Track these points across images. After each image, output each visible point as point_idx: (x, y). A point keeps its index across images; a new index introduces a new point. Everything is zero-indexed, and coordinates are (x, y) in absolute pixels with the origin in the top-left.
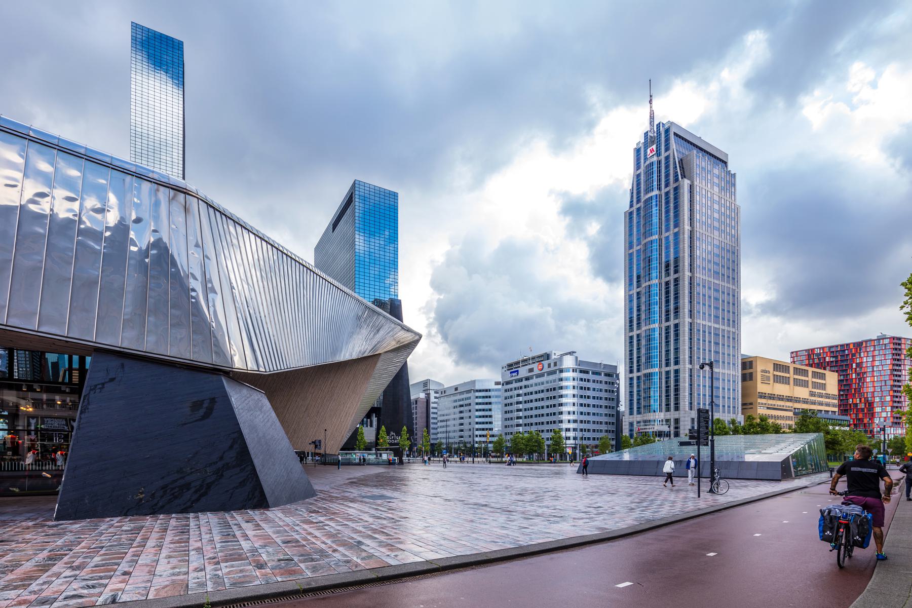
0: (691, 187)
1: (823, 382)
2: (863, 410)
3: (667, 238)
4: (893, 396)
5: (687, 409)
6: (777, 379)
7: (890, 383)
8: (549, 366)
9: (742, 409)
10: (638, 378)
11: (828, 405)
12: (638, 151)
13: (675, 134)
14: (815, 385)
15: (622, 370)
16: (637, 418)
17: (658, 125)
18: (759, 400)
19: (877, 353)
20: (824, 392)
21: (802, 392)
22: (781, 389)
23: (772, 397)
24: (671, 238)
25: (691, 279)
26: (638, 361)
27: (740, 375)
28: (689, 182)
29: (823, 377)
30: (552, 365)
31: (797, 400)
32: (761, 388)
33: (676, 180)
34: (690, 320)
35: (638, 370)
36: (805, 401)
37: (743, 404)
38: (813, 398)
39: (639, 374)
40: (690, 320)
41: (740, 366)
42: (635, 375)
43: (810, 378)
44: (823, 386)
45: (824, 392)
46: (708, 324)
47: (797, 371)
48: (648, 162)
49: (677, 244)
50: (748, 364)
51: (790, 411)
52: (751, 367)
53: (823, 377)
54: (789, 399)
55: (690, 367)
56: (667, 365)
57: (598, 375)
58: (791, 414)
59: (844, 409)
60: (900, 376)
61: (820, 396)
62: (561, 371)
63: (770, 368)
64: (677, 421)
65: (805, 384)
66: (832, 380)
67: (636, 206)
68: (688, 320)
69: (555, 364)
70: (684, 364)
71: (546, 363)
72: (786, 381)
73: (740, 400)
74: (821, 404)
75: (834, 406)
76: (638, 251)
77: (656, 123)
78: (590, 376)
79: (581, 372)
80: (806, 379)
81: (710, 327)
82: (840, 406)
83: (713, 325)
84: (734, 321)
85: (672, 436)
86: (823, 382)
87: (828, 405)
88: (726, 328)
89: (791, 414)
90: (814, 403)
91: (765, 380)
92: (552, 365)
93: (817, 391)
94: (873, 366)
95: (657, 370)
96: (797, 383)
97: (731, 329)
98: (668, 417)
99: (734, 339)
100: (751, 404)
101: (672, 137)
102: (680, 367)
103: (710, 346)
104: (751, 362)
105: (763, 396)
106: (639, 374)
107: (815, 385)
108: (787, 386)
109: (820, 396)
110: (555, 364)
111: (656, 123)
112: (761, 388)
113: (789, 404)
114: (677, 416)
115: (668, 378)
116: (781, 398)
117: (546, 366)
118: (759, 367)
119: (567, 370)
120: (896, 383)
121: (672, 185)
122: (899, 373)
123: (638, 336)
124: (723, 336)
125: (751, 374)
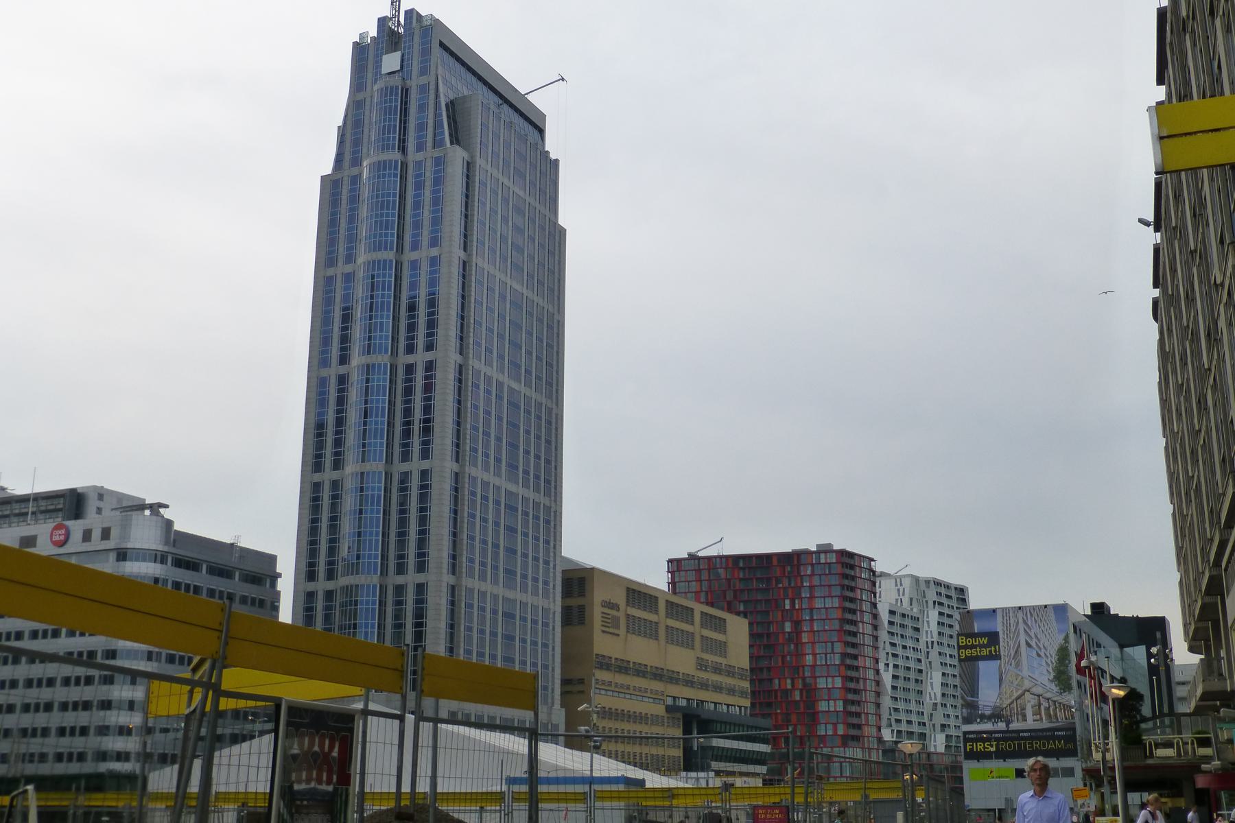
0: (469, 165)
3: (414, 265)
4: (846, 702)
6: (636, 627)
7: (839, 647)
8: (87, 535)
9: (562, 694)
10: (329, 595)
12: (360, 50)
13: (442, 44)
15: (287, 569)
17: (410, 13)
19: (816, 581)
21: (682, 660)
22: (641, 650)
23: (623, 667)
24: (424, 268)
25: (461, 369)
26: (334, 507)
27: (559, 610)
28: (466, 155)
29: (720, 625)
30: (96, 534)
31: (672, 678)
32: (604, 645)
33: (438, 143)
35: (330, 575)
36: (689, 682)
37: (565, 682)
40: (456, 467)
41: (559, 589)
42: (321, 585)
43: (696, 628)
44: (721, 648)
46: (488, 587)
47: (674, 609)
49: (438, 181)
50: (578, 582)
52: (582, 594)
53: (720, 625)
56: (410, 349)
59: (764, 696)
61: (717, 669)
63: (620, 598)
65: (685, 640)
66: (738, 630)
67: (348, 171)
68: (450, 465)
69: (106, 534)
71: (77, 527)
72: (650, 630)
73: (558, 671)
74: (718, 688)
75: (743, 694)
76: (415, 246)
77: (404, 7)
83: (500, 591)
84: (548, 482)
88: (531, 495)
89: (660, 710)
90: (704, 686)
91: (611, 624)
92: (96, 534)
94: (811, 609)
96: (675, 637)
99: (547, 522)
100: (581, 681)
103: (496, 556)
105: (605, 664)
106: (330, 585)
108: (653, 643)
109: (717, 669)
110: (106, 534)
111: (404, 7)
112: (604, 645)
113: (657, 686)
117: (76, 535)
118: (599, 595)
120: (849, 616)
121: (430, 153)
122: (852, 628)
123: (336, 485)
124: (526, 514)
125: (582, 609)
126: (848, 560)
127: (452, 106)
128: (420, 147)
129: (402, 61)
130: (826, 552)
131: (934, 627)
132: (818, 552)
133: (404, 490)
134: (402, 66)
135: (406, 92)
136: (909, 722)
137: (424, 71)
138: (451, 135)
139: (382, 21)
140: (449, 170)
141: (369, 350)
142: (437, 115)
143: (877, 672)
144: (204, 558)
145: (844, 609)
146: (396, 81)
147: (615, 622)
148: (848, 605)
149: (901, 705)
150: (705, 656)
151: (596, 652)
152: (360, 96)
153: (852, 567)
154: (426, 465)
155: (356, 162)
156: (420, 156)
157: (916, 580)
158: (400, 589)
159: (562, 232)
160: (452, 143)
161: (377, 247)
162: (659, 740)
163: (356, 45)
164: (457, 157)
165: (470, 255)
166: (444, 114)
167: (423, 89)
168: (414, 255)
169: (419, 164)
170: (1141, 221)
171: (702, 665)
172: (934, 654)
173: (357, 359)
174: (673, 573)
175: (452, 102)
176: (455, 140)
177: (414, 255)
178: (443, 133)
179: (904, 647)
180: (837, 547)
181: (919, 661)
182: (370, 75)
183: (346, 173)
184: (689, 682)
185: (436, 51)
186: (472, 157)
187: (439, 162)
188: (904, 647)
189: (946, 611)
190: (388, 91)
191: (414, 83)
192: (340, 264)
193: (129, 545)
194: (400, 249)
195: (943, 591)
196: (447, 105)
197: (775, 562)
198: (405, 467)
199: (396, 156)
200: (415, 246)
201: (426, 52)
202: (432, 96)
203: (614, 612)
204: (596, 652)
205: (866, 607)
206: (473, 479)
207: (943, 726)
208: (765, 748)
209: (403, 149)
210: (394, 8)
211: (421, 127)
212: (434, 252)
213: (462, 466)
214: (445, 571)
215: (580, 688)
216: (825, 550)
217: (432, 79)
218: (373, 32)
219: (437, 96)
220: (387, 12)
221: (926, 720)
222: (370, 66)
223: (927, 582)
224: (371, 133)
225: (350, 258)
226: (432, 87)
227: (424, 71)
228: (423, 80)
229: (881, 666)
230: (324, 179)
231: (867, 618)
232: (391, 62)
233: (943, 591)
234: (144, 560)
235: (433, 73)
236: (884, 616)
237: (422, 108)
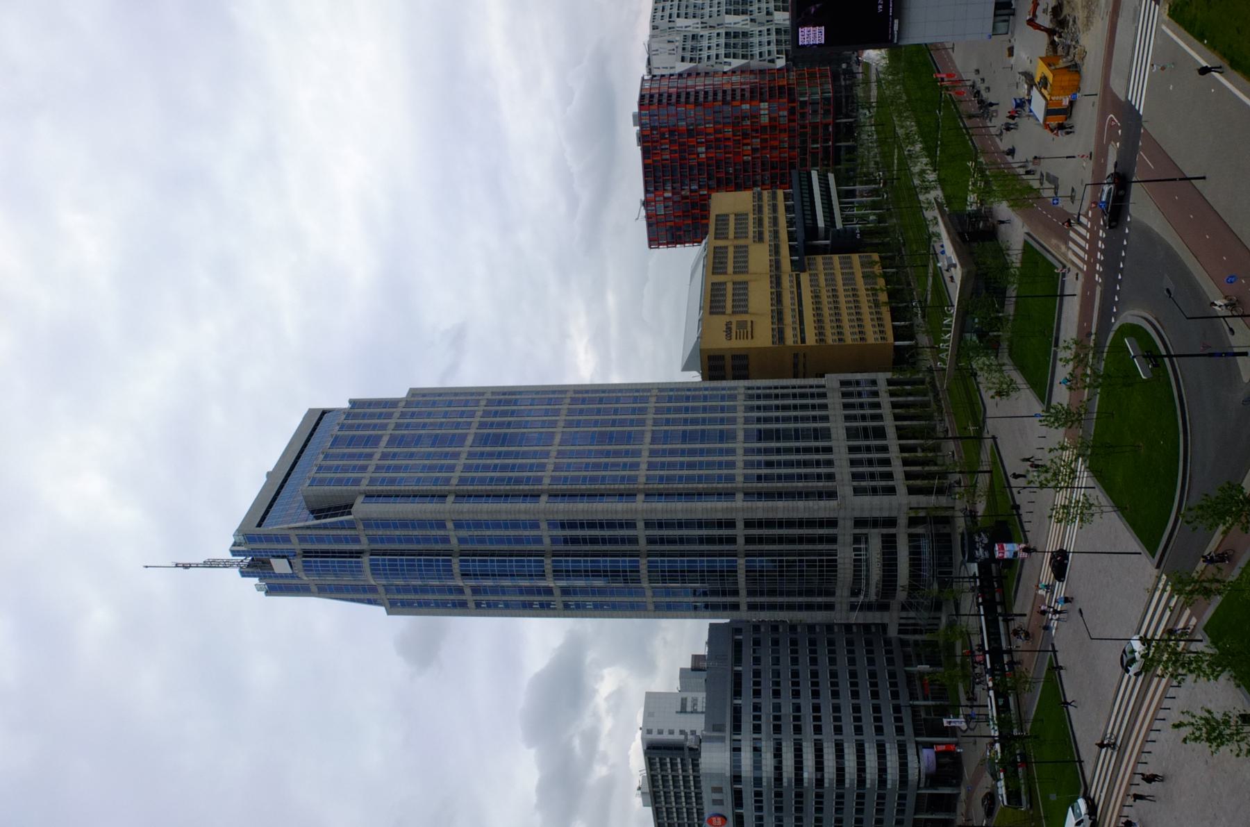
0: (369, 496)
1: (732, 218)
2: (763, 141)
5: (833, 503)
6: (741, 305)
8: (719, 802)
11: (774, 208)
12: (272, 590)
13: (259, 525)
14: (741, 233)
16: (842, 594)
17: (234, 553)
18: (790, 340)
20: (751, 216)
21: (759, 257)
22: (760, 298)
24: (464, 533)
29: (722, 219)
30: (717, 796)
31: (776, 265)
32: (763, 338)
33: (351, 525)
34: (640, 497)
35: (736, 593)
36: (776, 250)
38: (767, 235)
39: (743, 592)
40: (640, 497)
44: (741, 218)
45: (751, 216)
46: (644, 459)
48: (301, 574)
50: (713, 364)
51: (798, 277)
52: (722, 358)
54: (777, 281)
55: (740, 496)
57: (728, 675)
58: (805, 277)
60: (706, 93)
62: (737, 778)
63: (720, 321)
64: (859, 523)
65: (742, 252)
67: (382, 594)
70: (737, 509)
72: (742, 289)
74: (775, 221)
75: (774, 197)
76: (446, 540)
78: (746, 702)
79: (737, 728)
80: (731, 250)
81: (653, 453)
82: (773, 186)
85: (892, 531)
86: (732, 218)
87: (774, 208)
89: (805, 277)
90: (776, 234)
91: (746, 330)
93: (751, 229)
95: (741, 562)
96: (742, 266)
97: (652, 404)
98: (850, 539)
100: (796, 356)
101: (264, 530)
102: (740, 519)
104: (711, 358)
105: (779, 334)
107: (741, 233)
108: (751, 286)
109: (760, 222)
111: (229, 556)
112: (763, 338)
113: (786, 282)
114: (850, 523)
115: (760, 540)
116: (778, 298)
118: (721, 343)
119: (736, 764)
121: (361, 532)
122: (702, 95)
125: (734, 357)
126: (646, 101)
127: (318, 512)
128: (356, 540)
129: (278, 557)
130: (640, 119)
131: (690, 22)
132: (642, 125)
133: (662, 541)
134: (283, 557)
135: (307, 553)
136: (769, 43)
137: (286, 539)
138: (342, 514)
139: (244, 574)
140: (375, 516)
141: (542, 575)
142: (325, 527)
143: (733, 72)
144: (729, 703)
145: (687, 102)
146: (298, 562)
147: (742, 325)
148: (683, 100)
149: (756, 51)
150: (751, 234)
151: (770, 345)
152: (314, 588)
153: (652, 96)
154: (641, 525)
155: (373, 589)
156: (364, 540)
157: (652, 36)
158: (749, 540)
159: (414, 393)
160: (349, 513)
161: (449, 572)
162: (831, 279)
163: (267, 593)
164: (362, 509)
165: (450, 492)
166: (323, 521)
167: (302, 539)
168: (454, 541)
169: (372, 540)
170: (1245, 354)
171: (760, 238)
172: (712, 22)
173: (550, 583)
174: (660, 244)
175: (312, 512)
176: (346, 508)
177: (454, 541)
178: (342, 522)
179: (709, 48)
180: (636, 109)
181: (718, 34)
182: (294, 582)
183: (362, 533)
184: (776, 250)
185: (264, 530)
186: (361, 493)
187: (368, 523)
188: (709, 48)
189: (675, 11)
190: (307, 568)
191: (297, 546)
192: (464, 598)
193: (728, 774)
194: (449, 553)
195: (659, 14)
196: (317, 518)
197: (650, 161)
198: (642, 541)
199: (366, 560)
200: (446, 540)
201: (268, 538)
202: (309, 532)
203: (734, 327)
204: (770, 345)
205: (682, 83)
206: (554, 480)
207: (768, 13)
208: (814, 175)
209: (358, 554)
210: (231, 566)
211: (338, 539)
212: (450, 525)
213: (639, 491)
214: (734, 504)
215: (801, 358)
216: (638, 119)
217: (292, 532)
218: (256, 580)
219: (308, 528)
220: (235, 572)
221: (764, 28)
222: (286, 581)
223: (654, 28)
224: (347, 580)
225: (460, 590)
226: (300, 532)
227: (286, 539)
228: (295, 540)
229: (726, 68)
230: (389, 613)
231: (690, 83)
232: (281, 566)
233: (659, 14)
234: (740, 761)
235: (287, 532)
236: (687, 66)
237: (320, 540)
